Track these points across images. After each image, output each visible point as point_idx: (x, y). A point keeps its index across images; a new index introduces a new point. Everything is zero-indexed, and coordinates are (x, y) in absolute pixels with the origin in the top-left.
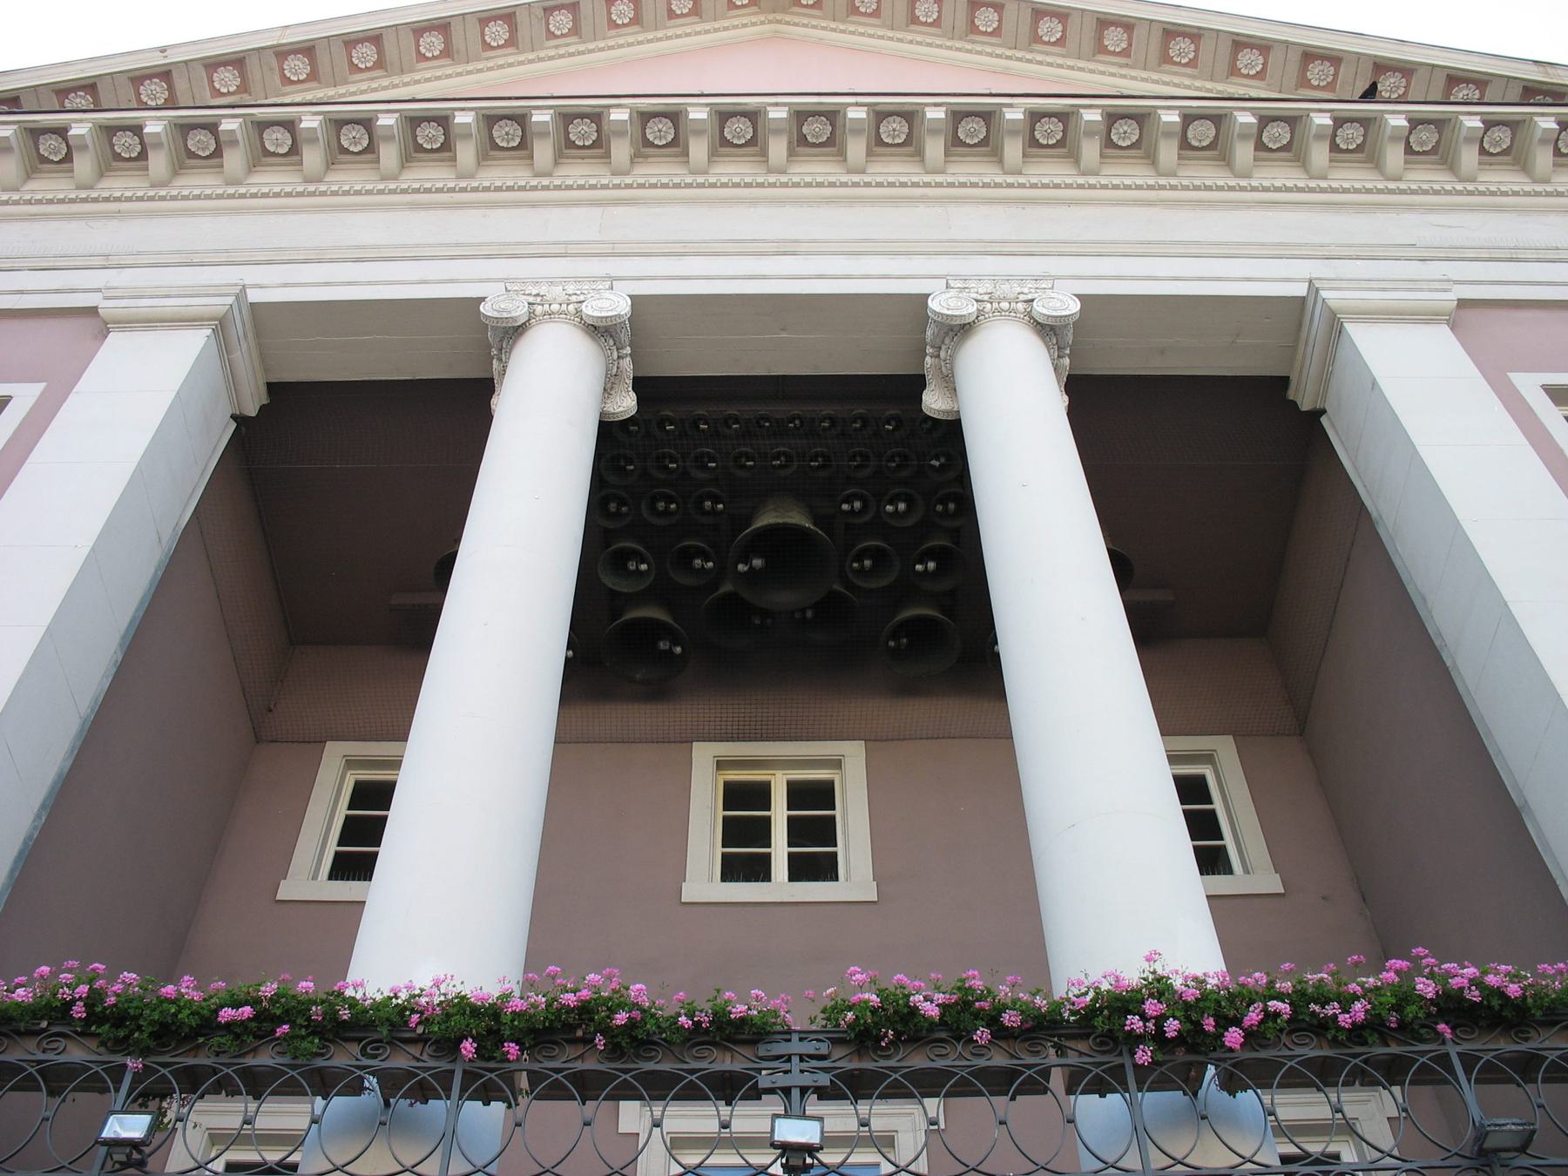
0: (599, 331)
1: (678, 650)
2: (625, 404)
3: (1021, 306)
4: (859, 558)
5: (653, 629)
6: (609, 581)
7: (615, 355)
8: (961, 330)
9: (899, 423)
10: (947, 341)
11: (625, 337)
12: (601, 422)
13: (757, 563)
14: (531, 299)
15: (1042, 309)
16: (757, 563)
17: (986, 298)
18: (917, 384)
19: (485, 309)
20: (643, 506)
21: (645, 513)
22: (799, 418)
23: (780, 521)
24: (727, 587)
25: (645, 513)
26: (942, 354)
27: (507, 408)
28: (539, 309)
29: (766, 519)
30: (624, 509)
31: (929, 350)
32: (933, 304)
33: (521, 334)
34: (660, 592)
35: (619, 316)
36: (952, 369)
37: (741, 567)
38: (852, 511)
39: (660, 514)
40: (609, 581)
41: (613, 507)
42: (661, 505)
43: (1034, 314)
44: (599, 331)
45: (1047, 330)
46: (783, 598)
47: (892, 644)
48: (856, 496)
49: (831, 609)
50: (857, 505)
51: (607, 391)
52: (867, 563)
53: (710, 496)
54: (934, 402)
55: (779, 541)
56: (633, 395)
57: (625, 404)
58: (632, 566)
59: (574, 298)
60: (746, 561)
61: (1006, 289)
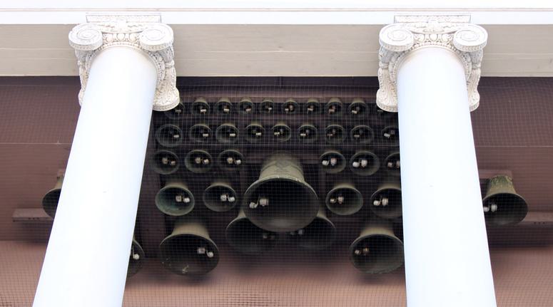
0: (153, 54)
1: (211, 254)
2: (171, 99)
3: (445, 38)
4: (335, 195)
5: (194, 241)
6: (164, 208)
7: (163, 67)
8: (404, 55)
9: (362, 108)
10: (393, 59)
11: (170, 55)
12: (153, 111)
13: (264, 202)
14: (104, 30)
15: (460, 41)
16: (264, 202)
17: (421, 30)
18: (371, 84)
19: (73, 37)
20: (186, 161)
21: (188, 165)
22: (292, 104)
23: (278, 177)
24: (242, 215)
25: (188, 165)
26: (390, 67)
27: (86, 97)
28: (110, 37)
29: (270, 173)
30: (173, 163)
31: (381, 64)
32: (384, 37)
33: (98, 54)
34: (200, 215)
35: (165, 44)
36: (396, 78)
37: (252, 205)
38: (360, 167)
39: (197, 166)
40: (164, 208)
41: (165, 160)
42: (198, 160)
43: (454, 43)
44: (153, 54)
45: (463, 55)
46: (281, 224)
47: (357, 252)
48: (363, 157)
49: (316, 229)
50: (364, 163)
51: (158, 90)
52: (341, 199)
53: (232, 155)
54: (384, 100)
55: (279, 189)
56: (177, 92)
57: (171, 99)
58: (178, 199)
59: (134, 29)
60: (256, 200)
61: (435, 25)
